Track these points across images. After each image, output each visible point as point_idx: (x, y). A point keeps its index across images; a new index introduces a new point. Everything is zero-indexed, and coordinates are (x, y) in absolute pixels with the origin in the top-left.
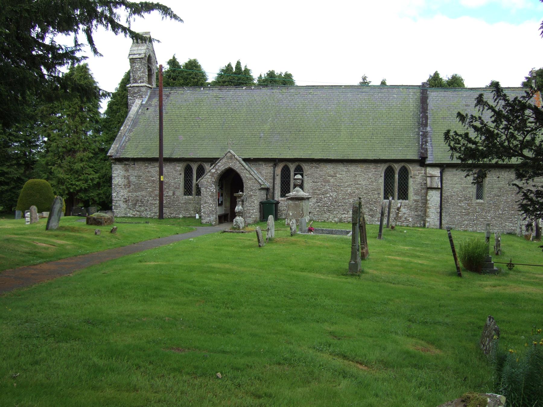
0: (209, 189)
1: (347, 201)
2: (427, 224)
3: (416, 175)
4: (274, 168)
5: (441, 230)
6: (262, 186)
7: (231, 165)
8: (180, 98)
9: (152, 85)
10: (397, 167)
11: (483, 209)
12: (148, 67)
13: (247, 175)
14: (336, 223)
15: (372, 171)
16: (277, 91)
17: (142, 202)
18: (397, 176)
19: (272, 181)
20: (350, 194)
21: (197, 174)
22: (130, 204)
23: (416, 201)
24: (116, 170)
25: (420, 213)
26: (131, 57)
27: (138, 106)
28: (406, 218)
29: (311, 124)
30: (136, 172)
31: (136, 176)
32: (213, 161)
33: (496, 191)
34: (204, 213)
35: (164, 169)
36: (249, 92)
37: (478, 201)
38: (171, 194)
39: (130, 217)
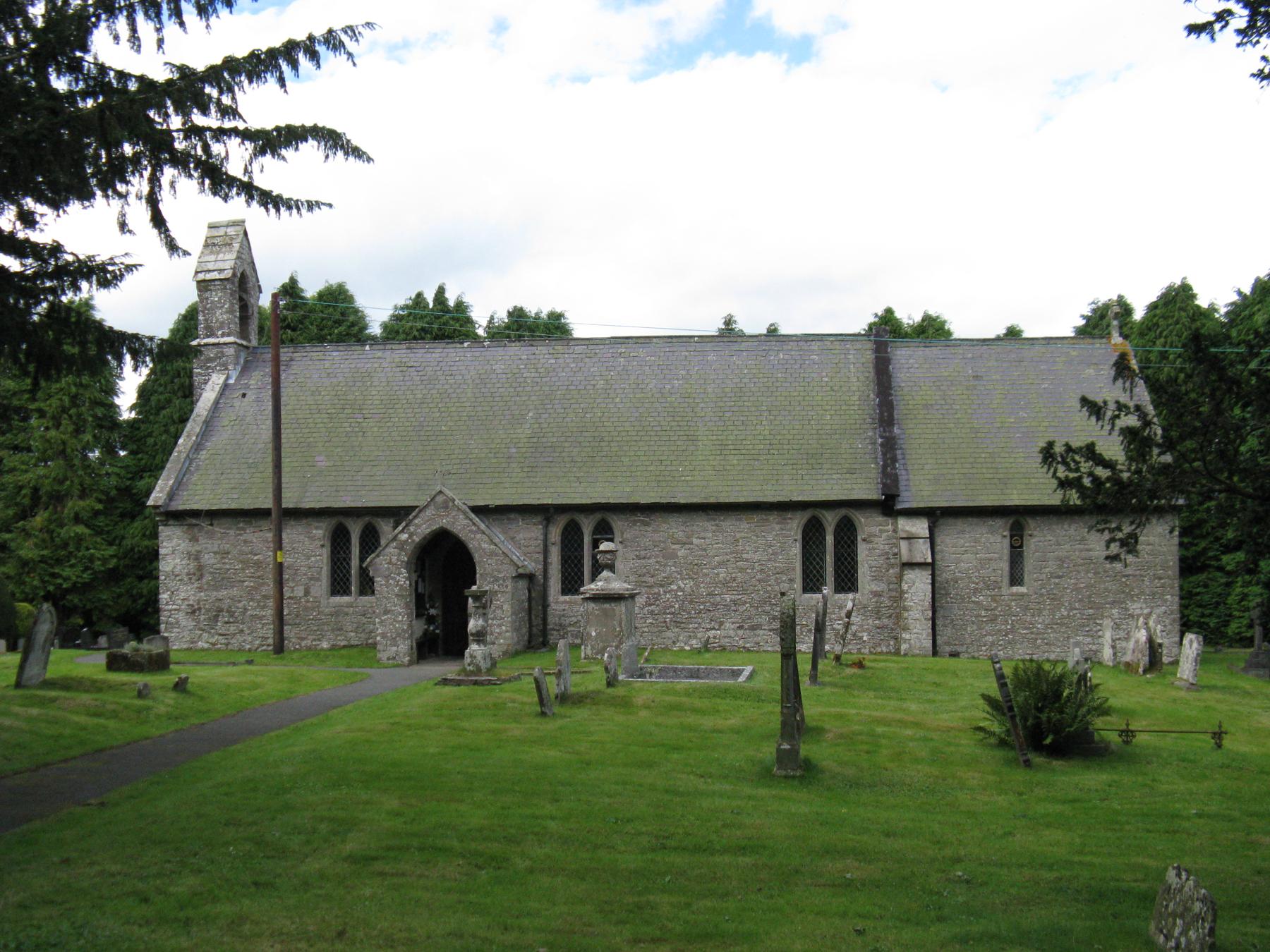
0: (393, 578)
1: (718, 599)
2: (904, 647)
3: (875, 539)
4: (546, 527)
5: (937, 659)
6: (521, 571)
7: (445, 522)
8: (315, 370)
9: (250, 341)
10: (830, 520)
11: (1026, 608)
12: (241, 299)
13: (485, 546)
14: (699, 652)
15: (773, 529)
16: (544, 350)
17: (232, 614)
18: (830, 539)
19: (541, 558)
20: (725, 584)
21: (361, 545)
22: (202, 617)
23: (876, 594)
24: (170, 539)
25: (886, 621)
26: (201, 277)
27: (217, 388)
28: (854, 635)
29: (627, 424)
30: (215, 545)
31: (215, 553)
32: (399, 514)
33: (1052, 567)
34: (383, 635)
35: (284, 536)
36: (477, 354)
37: (1015, 589)
38: (301, 594)
39: (203, 650)
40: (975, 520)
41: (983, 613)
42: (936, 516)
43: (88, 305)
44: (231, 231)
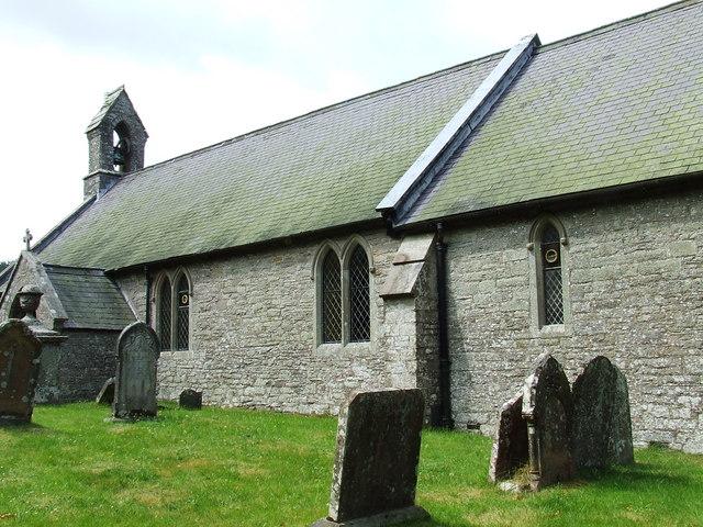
37: (548, 329)
40: (494, 230)
41: (507, 365)
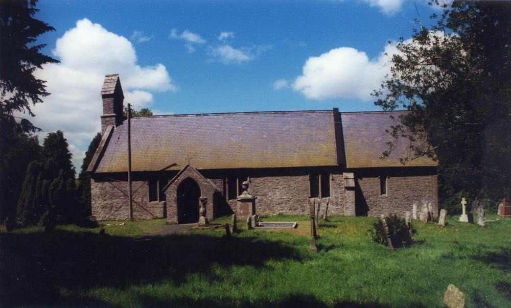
23: (337, 198)
26: (103, 93)
38: (140, 201)
42: (361, 173)
43: (373, 53)
44: (113, 78)
